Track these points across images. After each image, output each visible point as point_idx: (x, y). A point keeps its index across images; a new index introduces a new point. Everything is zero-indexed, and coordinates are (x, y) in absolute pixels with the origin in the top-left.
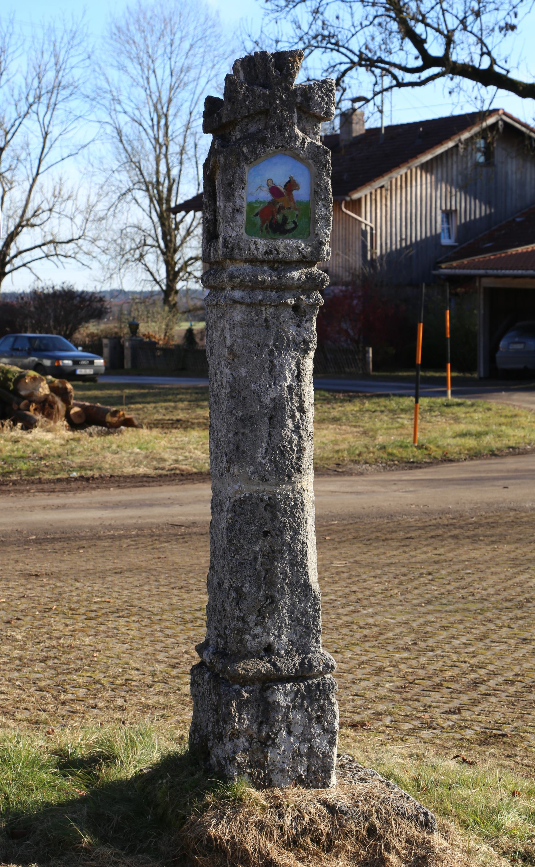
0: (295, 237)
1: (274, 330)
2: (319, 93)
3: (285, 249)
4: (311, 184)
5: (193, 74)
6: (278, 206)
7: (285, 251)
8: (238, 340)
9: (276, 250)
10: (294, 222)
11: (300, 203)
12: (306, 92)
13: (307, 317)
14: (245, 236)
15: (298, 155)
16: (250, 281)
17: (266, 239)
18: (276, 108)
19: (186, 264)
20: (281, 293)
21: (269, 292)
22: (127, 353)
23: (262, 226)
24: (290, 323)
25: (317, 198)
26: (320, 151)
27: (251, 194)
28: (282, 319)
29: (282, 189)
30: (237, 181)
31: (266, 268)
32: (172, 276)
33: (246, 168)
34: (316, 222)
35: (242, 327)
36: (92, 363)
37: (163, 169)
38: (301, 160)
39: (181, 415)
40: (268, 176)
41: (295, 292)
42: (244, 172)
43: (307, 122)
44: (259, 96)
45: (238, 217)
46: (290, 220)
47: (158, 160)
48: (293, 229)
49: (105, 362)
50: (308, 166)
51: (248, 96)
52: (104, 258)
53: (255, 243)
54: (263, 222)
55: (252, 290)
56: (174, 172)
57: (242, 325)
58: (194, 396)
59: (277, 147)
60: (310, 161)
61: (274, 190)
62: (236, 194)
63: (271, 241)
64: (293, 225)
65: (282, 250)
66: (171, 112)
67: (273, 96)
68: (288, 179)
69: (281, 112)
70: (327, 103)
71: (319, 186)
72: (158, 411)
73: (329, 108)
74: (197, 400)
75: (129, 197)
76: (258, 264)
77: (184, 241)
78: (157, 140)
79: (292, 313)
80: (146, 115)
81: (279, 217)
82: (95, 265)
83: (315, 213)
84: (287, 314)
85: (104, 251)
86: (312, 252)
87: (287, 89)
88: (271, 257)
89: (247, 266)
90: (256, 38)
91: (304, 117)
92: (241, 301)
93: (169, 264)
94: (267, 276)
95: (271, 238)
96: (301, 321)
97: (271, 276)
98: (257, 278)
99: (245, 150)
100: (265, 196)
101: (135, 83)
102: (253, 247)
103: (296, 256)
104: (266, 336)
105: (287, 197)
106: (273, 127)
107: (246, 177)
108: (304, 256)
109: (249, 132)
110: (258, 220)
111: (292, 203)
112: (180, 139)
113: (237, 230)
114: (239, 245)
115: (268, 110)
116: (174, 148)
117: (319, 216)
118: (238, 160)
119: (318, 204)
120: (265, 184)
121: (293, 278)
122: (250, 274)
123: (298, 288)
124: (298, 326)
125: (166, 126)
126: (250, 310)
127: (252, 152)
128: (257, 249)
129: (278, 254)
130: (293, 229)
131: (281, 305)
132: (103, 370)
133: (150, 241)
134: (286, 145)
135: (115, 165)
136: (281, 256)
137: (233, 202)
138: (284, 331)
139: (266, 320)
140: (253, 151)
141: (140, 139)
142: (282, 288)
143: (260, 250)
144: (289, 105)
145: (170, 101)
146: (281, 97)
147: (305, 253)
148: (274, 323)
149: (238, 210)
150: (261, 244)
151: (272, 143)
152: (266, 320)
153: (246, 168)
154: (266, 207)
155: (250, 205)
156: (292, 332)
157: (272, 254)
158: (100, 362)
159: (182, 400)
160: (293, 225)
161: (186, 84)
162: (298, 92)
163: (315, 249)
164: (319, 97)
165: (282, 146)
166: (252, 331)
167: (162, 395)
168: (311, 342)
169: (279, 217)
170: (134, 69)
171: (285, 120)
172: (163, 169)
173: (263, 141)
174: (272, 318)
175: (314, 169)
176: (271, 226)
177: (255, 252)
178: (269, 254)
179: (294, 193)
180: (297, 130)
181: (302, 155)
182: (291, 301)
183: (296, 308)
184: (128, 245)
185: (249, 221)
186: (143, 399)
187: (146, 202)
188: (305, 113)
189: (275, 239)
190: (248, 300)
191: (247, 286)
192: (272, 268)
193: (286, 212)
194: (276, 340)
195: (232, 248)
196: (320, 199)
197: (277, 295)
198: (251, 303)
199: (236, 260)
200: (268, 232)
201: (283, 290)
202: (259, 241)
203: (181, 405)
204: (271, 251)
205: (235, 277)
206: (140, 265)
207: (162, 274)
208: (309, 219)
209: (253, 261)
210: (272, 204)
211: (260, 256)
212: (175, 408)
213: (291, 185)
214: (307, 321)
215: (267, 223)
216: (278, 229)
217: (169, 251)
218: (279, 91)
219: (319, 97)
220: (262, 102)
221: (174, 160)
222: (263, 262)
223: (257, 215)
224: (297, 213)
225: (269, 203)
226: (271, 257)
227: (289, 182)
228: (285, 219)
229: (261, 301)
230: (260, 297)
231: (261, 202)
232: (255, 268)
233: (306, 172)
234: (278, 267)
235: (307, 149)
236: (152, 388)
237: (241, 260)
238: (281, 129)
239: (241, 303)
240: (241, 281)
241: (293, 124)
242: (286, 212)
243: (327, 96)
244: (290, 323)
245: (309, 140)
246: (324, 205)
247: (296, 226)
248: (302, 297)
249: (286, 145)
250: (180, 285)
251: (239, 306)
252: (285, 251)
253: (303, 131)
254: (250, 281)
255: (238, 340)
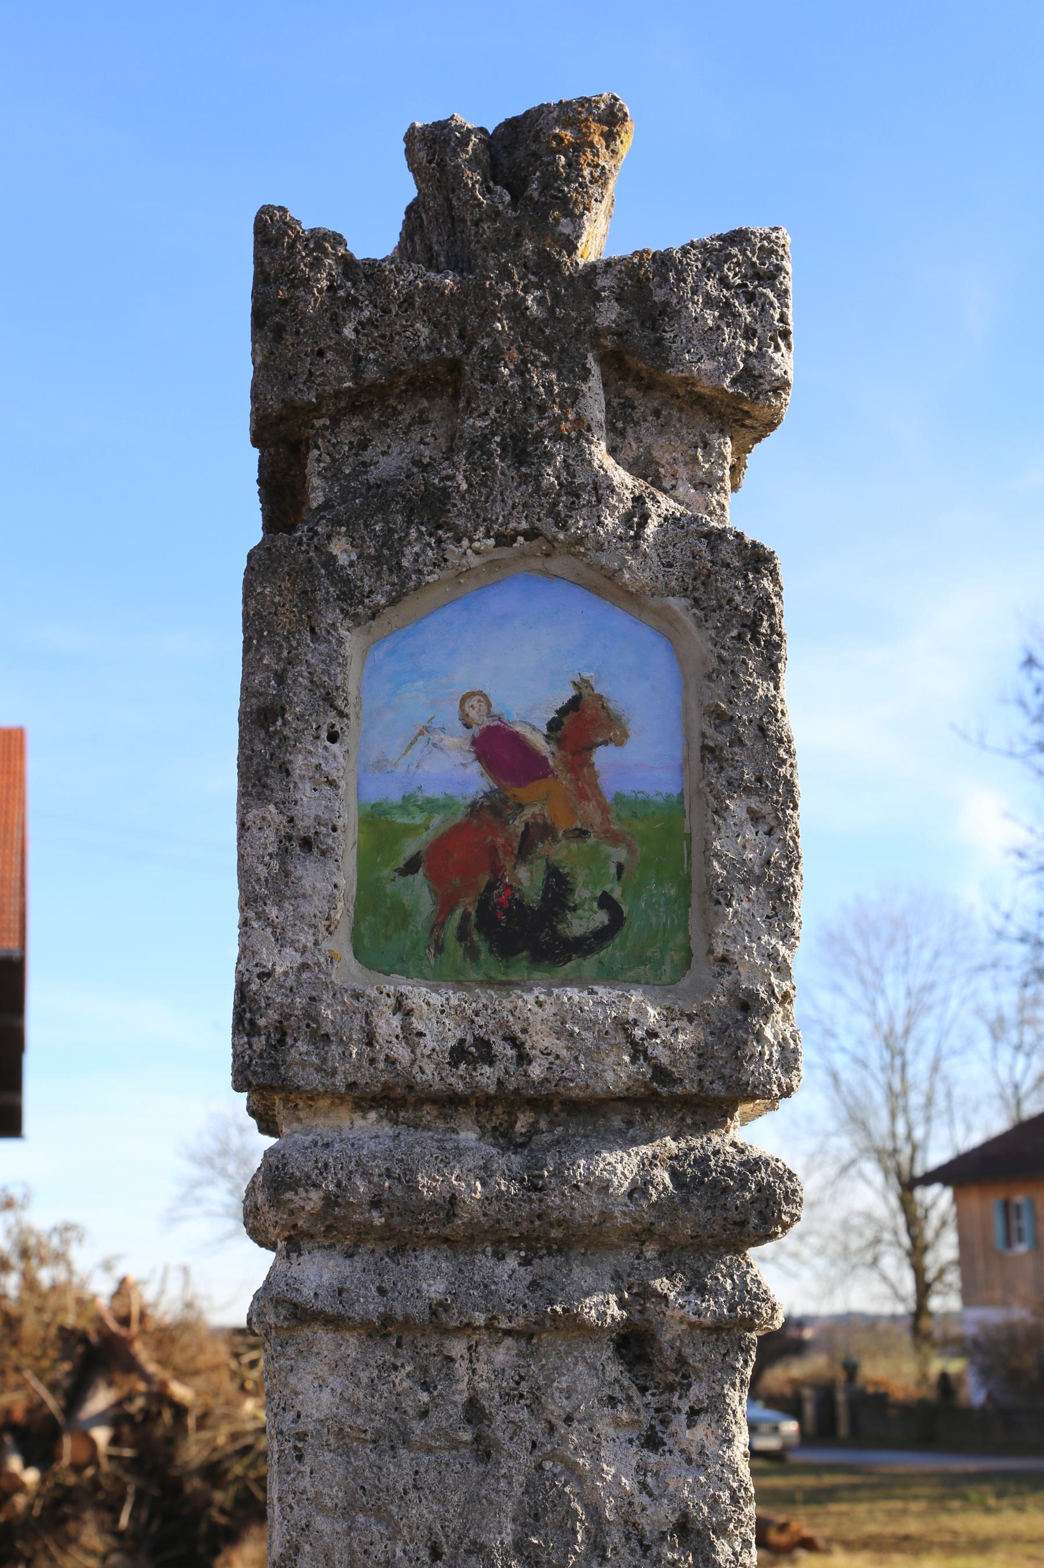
0: (610, 977)
1: (516, 1463)
2: (711, 286)
3: (559, 1034)
4: (685, 712)
5: (939, 993)
6: (518, 825)
7: (559, 1047)
8: (321, 1523)
9: (512, 1040)
10: (606, 902)
11: (636, 807)
12: (645, 281)
13: (697, 1392)
14: (348, 971)
15: (612, 576)
16: (376, 1204)
17: (460, 984)
18: (494, 356)
19: (942, 1272)
20: (547, 1265)
21: (484, 1262)
22: (842, 1412)
23: (438, 925)
24: (605, 1428)
25: (720, 783)
26: (726, 552)
27: (381, 765)
28: (556, 1406)
29: (539, 741)
30: (300, 699)
31: (468, 1136)
32: (923, 1289)
33: (352, 642)
34: (719, 897)
35: (346, 1451)
36: (776, 1429)
37: (901, 1128)
38: (631, 599)
39: (912, 1526)
40: (465, 677)
41: (626, 1258)
42: (335, 659)
43: (662, 429)
44: (408, 301)
45: (309, 874)
46: (582, 893)
47: (893, 1116)
48: (602, 936)
49: (802, 1430)
50: (667, 627)
51: (352, 302)
52: (820, 1263)
53: (400, 1006)
54: (446, 905)
55: (400, 1250)
56: (919, 1133)
57: (344, 1439)
58: (939, 1491)
59: (504, 540)
60: (677, 604)
61: (497, 747)
62: (299, 763)
63: (485, 996)
64: (602, 918)
65: (540, 1039)
66: (910, 1047)
67: (476, 301)
68: (570, 693)
69: (521, 371)
70: (749, 334)
71: (721, 718)
72: (871, 1517)
73: (761, 354)
74: (942, 1498)
75: (853, 1171)
76: (428, 1113)
77: (938, 1234)
78: (890, 1088)
79: (614, 1370)
80: (875, 1054)
81: (528, 880)
82: (806, 1273)
83: (708, 854)
84: (584, 1377)
85: (820, 1252)
86: (702, 1054)
87: (546, 268)
88: (487, 1076)
89: (368, 1129)
90: (1005, 906)
91: (643, 405)
92: (328, 1305)
93: (919, 1271)
94: (466, 1172)
95: (489, 983)
96: (664, 1414)
97: (485, 1173)
98: (412, 1187)
99: (341, 550)
100: (455, 775)
101: (855, 1008)
102: (388, 1024)
103: (618, 1072)
104: (472, 1499)
105: (565, 780)
106: (480, 443)
107: (352, 680)
108: (660, 1073)
109: (374, 475)
110: (419, 894)
111: (590, 808)
112: (924, 1086)
113: (306, 939)
114: (311, 1016)
115: (455, 367)
116: (916, 1099)
117: (731, 866)
118: (307, 597)
119: (721, 811)
120: (450, 715)
121: (605, 1187)
122: (377, 1167)
123: (642, 1234)
124: (652, 1442)
125: (904, 1067)
126: (382, 1354)
127: (378, 559)
128: (410, 1036)
129: (523, 1059)
130: (602, 936)
131: (546, 1328)
132: (795, 1440)
133: (887, 1236)
134: (547, 526)
135: (831, 1125)
136: (536, 1071)
137: (282, 805)
138: (572, 1468)
139: (474, 1411)
140: (385, 557)
141: (863, 1084)
142: (547, 1237)
143: (429, 1042)
144: (559, 341)
145: (907, 1031)
146: (516, 307)
147: (664, 1057)
148: (517, 1427)
149: (307, 844)
150: (435, 1012)
151: (479, 515)
152: (474, 1411)
153: (352, 642)
154: (457, 829)
155: (376, 822)
156: (615, 1471)
157: (490, 1060)
158: (790, 1427)
159: (916, 1498)
160: (602, 918)
161: (930, 1008)
162: (602, 282)
163: (720, 1033)
164: (709, 302)
165: (531, 535)
166: (400, 1468)
167: (886, 1487)
168: (721, 1530)
169: (528, 880)
170: (852, 989)
171: (542, 409)
172: (901, 1128)
173: (431, 508)
174: (508, 1398)
175: (699, 642)
176: (486, 919)
177: (402, 1053)
178: (473, 1062)
179: (602, 757)
180: (600, 453)
181: (636, 573)
182: (604, 1307)
183: (633, 1344)
184: (855, 1243)
185: (370, 898)
186: (853, 1494)
187: (878, 1178)
188: (648, 386)
189: (506, 986)
190: (368, 1305)
191: (364, 1232)
192: (504, 1138)
193: (561, 852)
194: (531, 1517)
195: (281, 1035)
196: (734, 785)
197: (526, 1275)
198: (387, 1320)
199: (312, 1097)
200: (472, 953)
201: (561, 1248)
202: (420, 995)
203: (915, 1506)
204: (484, 1044)
205: (293, 1184)
206: (874, 1276)
207: (908, 1284)
208: (685, 885)
209: (394, 1098)
210: (488, 811)
211: (429, 1074)
212: (904, 1512)
213: (582, 722)
214: (694, 1413)
215: (468, 904)
216: (525, 934)
217: (917, 1253)
218: (506, 275)
219: (709, 302)
220: (424, 330)
221: (917, 1116)
222: (450, 1103)
223: (411, 867)
224: (620, 854)
225: (475, 809)
226: (487, 1076)
227: (574, 704)
228: (558, 886)
229: (437, 1309)
230: (435, 1289)
231: (431, 806)
232: (408, 1136)
233: (659, 660)
234: (534, 1130)
235: (661, 545)
236: (870, 1473)
237: (337, 1098)
238: (523, 451)
239: (335, 1322)
240: (330, 1201)
241: (583, 428)
242: (561, 852)
243: (751, 298)
244: (605, 1428)
245: (667, 504)
246: (755, 817)
247: (617, 919)
248: (661, 1284)
249: (547, 526)
250: (935, 1303)
251: (324, 1338)
252: (559, 1047)
253: (643, 467)
254: (376, 1204)
255: (321, 1523)
